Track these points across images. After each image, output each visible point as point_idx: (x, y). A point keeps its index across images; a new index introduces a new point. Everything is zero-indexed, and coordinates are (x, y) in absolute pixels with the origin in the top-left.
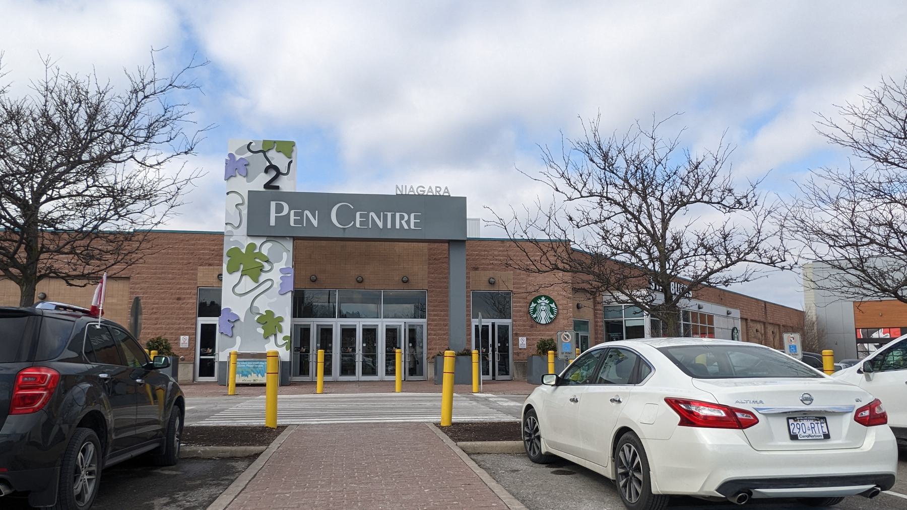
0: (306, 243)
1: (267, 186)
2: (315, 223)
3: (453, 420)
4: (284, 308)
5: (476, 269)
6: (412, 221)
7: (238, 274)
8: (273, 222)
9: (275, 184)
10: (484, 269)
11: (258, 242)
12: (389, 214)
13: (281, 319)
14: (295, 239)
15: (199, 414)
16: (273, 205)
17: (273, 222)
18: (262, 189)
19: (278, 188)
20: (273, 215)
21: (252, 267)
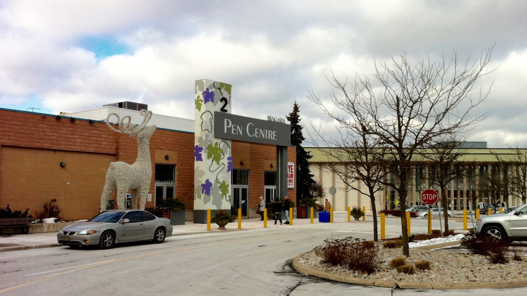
0: (74, 148)
1: (222, 109)
2: (241, 133)
3: (433, 228)
4: (226, 177)
5: (266, 159)
6: (274, 135)
7: (211, 159)
8: (225, 132)
9: (225, 109)
10: (269, 159)
11: (219, 141)
12: (266, 131)
13: (228, 186)
14: (233, 141)
15: (19, 247)
16: (226, 120)
17: (225, 132)
18: (219, 111)
19: (226, 111)
20: (226, 127)
21: (215, 154)
